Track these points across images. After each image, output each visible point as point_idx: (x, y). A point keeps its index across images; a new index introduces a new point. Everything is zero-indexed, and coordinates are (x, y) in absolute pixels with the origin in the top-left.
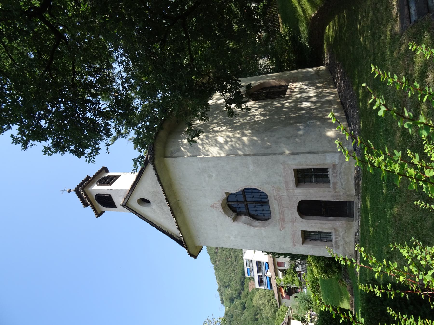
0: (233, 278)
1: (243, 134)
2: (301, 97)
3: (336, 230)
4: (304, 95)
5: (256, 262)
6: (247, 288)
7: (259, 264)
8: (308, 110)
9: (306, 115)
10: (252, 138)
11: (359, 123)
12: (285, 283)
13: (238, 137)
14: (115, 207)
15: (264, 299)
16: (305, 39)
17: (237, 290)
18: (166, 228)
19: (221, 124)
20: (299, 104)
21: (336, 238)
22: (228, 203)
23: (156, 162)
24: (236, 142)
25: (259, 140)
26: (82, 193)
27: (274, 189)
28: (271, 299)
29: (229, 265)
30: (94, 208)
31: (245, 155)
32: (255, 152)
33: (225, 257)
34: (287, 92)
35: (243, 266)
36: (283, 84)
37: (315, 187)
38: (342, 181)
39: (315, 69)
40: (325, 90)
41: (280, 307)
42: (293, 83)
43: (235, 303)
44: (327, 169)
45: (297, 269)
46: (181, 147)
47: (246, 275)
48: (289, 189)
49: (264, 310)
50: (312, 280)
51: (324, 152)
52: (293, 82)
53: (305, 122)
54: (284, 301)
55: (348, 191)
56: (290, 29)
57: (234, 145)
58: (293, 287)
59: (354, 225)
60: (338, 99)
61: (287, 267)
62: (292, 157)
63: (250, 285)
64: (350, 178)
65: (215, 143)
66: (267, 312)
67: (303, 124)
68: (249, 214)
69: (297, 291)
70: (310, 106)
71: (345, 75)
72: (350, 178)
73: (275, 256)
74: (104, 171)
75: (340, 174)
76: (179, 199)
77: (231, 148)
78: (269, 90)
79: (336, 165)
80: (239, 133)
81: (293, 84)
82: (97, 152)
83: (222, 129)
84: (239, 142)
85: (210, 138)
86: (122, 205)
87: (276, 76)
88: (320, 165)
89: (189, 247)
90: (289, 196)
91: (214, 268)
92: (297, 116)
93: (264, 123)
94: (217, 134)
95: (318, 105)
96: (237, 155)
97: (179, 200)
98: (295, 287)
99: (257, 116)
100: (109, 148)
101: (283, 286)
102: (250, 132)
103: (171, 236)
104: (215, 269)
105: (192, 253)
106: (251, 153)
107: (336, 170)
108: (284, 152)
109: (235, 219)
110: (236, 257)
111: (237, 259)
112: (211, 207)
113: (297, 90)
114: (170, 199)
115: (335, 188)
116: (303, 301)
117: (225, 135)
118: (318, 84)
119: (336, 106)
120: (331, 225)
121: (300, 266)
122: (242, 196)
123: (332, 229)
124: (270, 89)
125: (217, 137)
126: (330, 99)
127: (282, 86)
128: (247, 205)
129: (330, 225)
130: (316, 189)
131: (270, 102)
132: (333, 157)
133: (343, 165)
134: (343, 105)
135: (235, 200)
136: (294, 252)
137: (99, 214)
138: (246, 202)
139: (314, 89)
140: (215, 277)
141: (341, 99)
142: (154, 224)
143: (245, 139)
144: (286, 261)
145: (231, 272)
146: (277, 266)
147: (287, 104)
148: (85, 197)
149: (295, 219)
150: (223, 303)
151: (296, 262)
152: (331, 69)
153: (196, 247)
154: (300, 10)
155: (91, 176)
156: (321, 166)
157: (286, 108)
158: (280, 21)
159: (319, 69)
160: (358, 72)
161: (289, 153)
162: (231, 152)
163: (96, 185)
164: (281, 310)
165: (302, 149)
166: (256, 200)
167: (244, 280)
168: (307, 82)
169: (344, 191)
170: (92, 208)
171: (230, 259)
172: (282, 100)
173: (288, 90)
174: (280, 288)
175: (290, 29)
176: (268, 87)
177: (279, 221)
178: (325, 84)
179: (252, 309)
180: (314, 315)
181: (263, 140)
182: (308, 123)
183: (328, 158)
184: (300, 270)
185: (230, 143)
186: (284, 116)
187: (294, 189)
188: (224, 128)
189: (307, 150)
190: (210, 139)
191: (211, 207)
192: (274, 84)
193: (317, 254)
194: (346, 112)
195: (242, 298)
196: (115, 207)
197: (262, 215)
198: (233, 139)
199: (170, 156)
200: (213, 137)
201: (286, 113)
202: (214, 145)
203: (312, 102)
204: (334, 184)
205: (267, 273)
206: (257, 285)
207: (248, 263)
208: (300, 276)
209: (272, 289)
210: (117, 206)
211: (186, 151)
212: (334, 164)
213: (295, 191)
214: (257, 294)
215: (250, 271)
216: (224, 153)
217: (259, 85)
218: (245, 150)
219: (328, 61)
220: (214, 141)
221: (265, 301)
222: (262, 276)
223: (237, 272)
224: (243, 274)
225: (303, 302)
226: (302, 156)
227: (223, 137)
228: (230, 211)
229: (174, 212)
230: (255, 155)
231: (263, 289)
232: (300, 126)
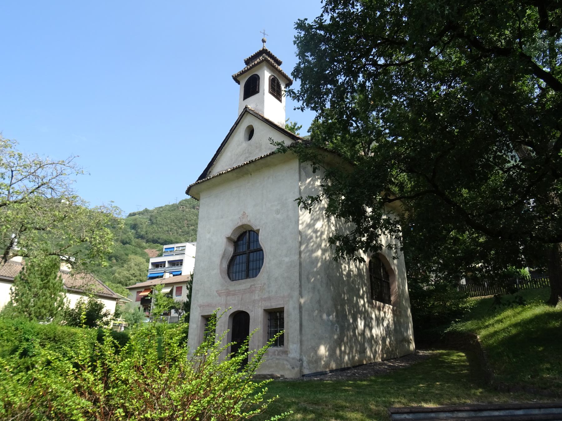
0: (162, 229)
1: (324, 251)
2: (372, 318)
4: (374, 323)
5: (182, 260)
6: (149, 247)
7: (180, 263)
8: (354, 326)
9: (346, 323)
10: (320, 260)
11: (331, 380)
12: (156, 295)
13: (321, 245)
14: (245, 98)
15: (136, 269)
16: (456, 327)
17: (146, 234)
18: (219, 158)
19: (339, 224)
20: (361, 316)
22: (248, 231)
24: (315, 243)
25: (317, 269)
26: (261, 58)
28: (136, 278)
29: (178, 224)
30: (243, 73)
31: (300, 253)
32: (304, 264)
33: (189, 219)
34: (380, 303)
35: (177, 243)
36: (393, 298)
37: (264, 331)
38: (270, 361)
39: (411, 337)
40: (381, 347)
41: (127, 289)
42: (392, 310)
43: (131, 232)
44: (283, 345)
45: (173, 311)
46: (310, 179)
47: (165, 247)
49: (123, 268)
50: (160, 329)
51: (301, 342)
52: (393, 311)
53: (337, 322)
54: (134, 294)
56: (470, 309)
57: (312, 240)
58: (152, 305)
60: (367, 362)
61: (176, 298)
62: (297, 306)
63: (153, 250)
65: (315, 219)
66: (121, 272)
67: (335, 319)
68: (236, 256)
69: (146, 311)
70: (359, 328)
71: (393, 369)
72: (272, 370)
73: (189, 284)
75: (277, 359)
77: (309, 237)
78: (384, 281)
79: (287, 354)
80: (326, 246)
81: (390, 311)
82: (294, 98)
83: (332, 226)
84: (315, 246)
85: (321, 212)
86: (246, 107)
87: (403, 291)
89: (199, 186)
90: (254, 301)
91: (174, 204)
92: (346, 312)
93: (338, 275)
94: (326, 220)
95: (360, 338)
96: (301, 244)
97: (251, 174)
98: (151, 308)
99: (347, 266)
100: (300, 110)
101: (153, 293)
102: (328, 258)
103: (211, 165)
104: (173, 205)
105: (192, 189)
106: (302, 260)
107: (281, 355)
108: (302, 297)
109: (229, 239)
110: (188, 233)
111: (185, 234)
113: (382, 314)
114: (252, 165)
116: (135, 317)
117: (325, 229)
118: (388, 340)
119: (357, 358)
121: (177, 315)
122: (255, 248)
124: (386, 282)
125: (322, 220)
126: (367, 352)
127: (390, 297)
128: (245, 254)
131: (366, 282)
132: (296, 352)
134: (359, 366)
135: (252, 240)
136: (193, 306)
137: (236, 79)
138: (249, 253)
139: (381, 335)
140: (163, 205)
141: (366, 364)
142: (225, 144)
143: (319, 253)
144: (183, 298)
145: (169, 226)
146: (177, 287)
147: (362, 302)
148: (256, 62)
150: (130, 215)
151: (182, 310)
152: (408, 356)
153: (198, 194)
154: (491, 321)
155: (280, 68)
157: (357, 300)
158: (487, 297)
159: (411, 343)
160: (389, 382)
161: (301, 303)
162: (303, 237)
163: (270, 75)
164: (123, 290)
165: (305, 317)
166: (251, 264)
167: (159, 243)
168: (392, 327)
170: (244, 70)
171: (185, 225)
172: (369, 296)
173: (382, 304)
174: (150, 289)
175: (470, 309)
176: (388, 280)
177: (227, 289)
178: (388, 348)
179: (122, 252)
180: (121, 329)
181: (318, 273)
182: (337, 325)
183: (295, 346)
184: (172, 315)
185: (314, 235)
186: (346, 298)
188: (333, 228)
189: (305, 323)
190: (320, 213)
192: (392, 288)
193: (190, 331)
194: (348, 368)
195: (137, 240)
196: (245, 98)
197: (234, 271)
198: (319, 239)
199: (301, 165)
200: (322, 216)
201: (350, 300)
202: (313, 217)
203: (364, 331)
205: (169, 274)
206: (153, 260)
207: (181, 248)
208: (165, 314)
209: (149, 279)
210: (246, 100)
211: (306, 185)
213: (260, 309)
214: (142, 260)
215: (171, 251)
216: (303, 229)
217: (392, 269)
218: (306, 253)
219: (421, 354)
220: (318, 217)
221: (134, 270)
222: (164, 266)
223: (169, 234)
224: (166, 243)
225: (133, 317)
227: (322, 227)
228: (239, 234)
229: (238, 170)
230: (300, 264)
231: (148, 268)
232: (333, 316)
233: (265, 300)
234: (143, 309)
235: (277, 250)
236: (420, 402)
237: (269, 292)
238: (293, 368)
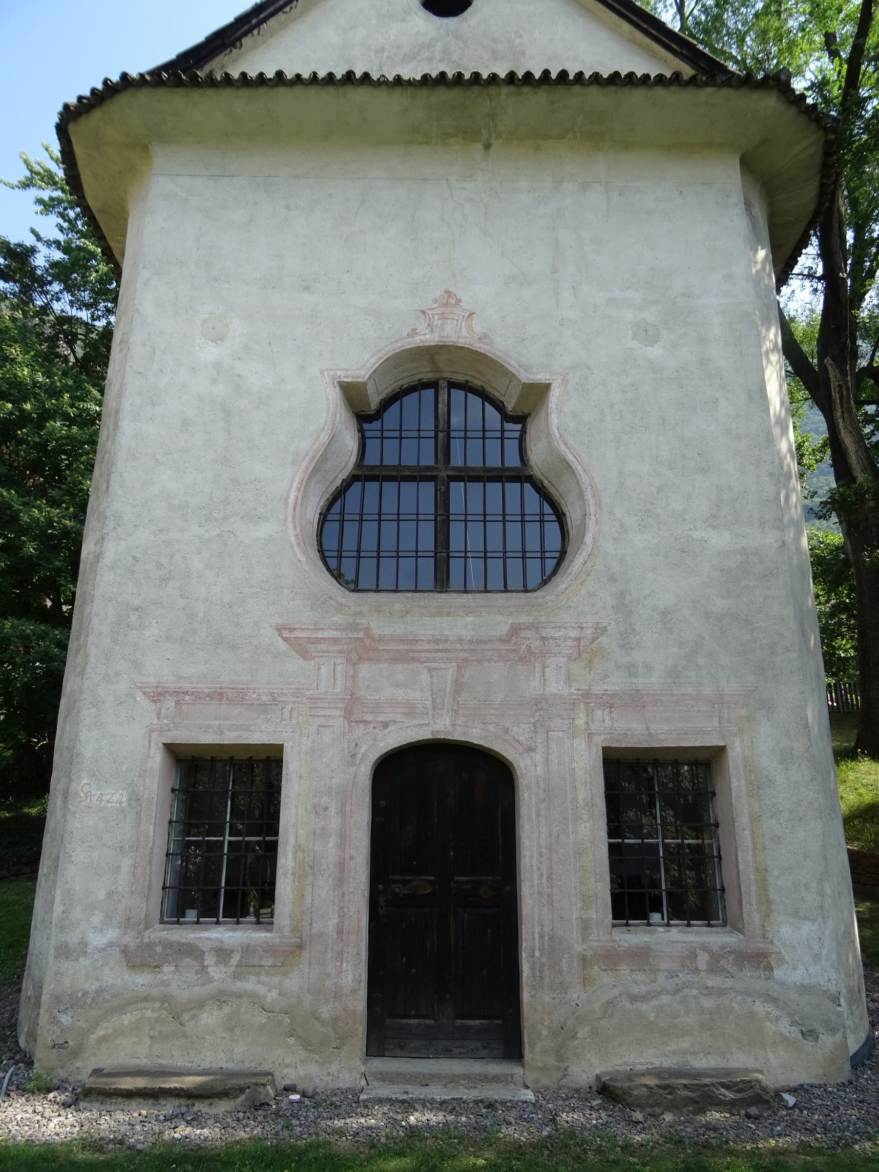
21: (223, 954)
27: (589, 632)
38: (665, 999)
48: (590, 713)
55: (595, 1033)
59: (334, 1068)
64: (685, 1043)
72: (685, 1043)
75: (709, 991)
76: (492, 150)
79: (769, 968)
90: (540, 703)
97: (487, 146)
107: (733, 970)
112: (448, 292)
120: (331, 931)
123: (295, 929)
132: (817, 958)
133: (770, 1008)
149: (368, 717)
169: (596, 1006)
183: (808, 928)
187: (590, 736)
212: (773, 960)
213: (580, 743)
233: (609, 703)
235: (660, 489)
237: (630, 669)
238: (810, 1034)
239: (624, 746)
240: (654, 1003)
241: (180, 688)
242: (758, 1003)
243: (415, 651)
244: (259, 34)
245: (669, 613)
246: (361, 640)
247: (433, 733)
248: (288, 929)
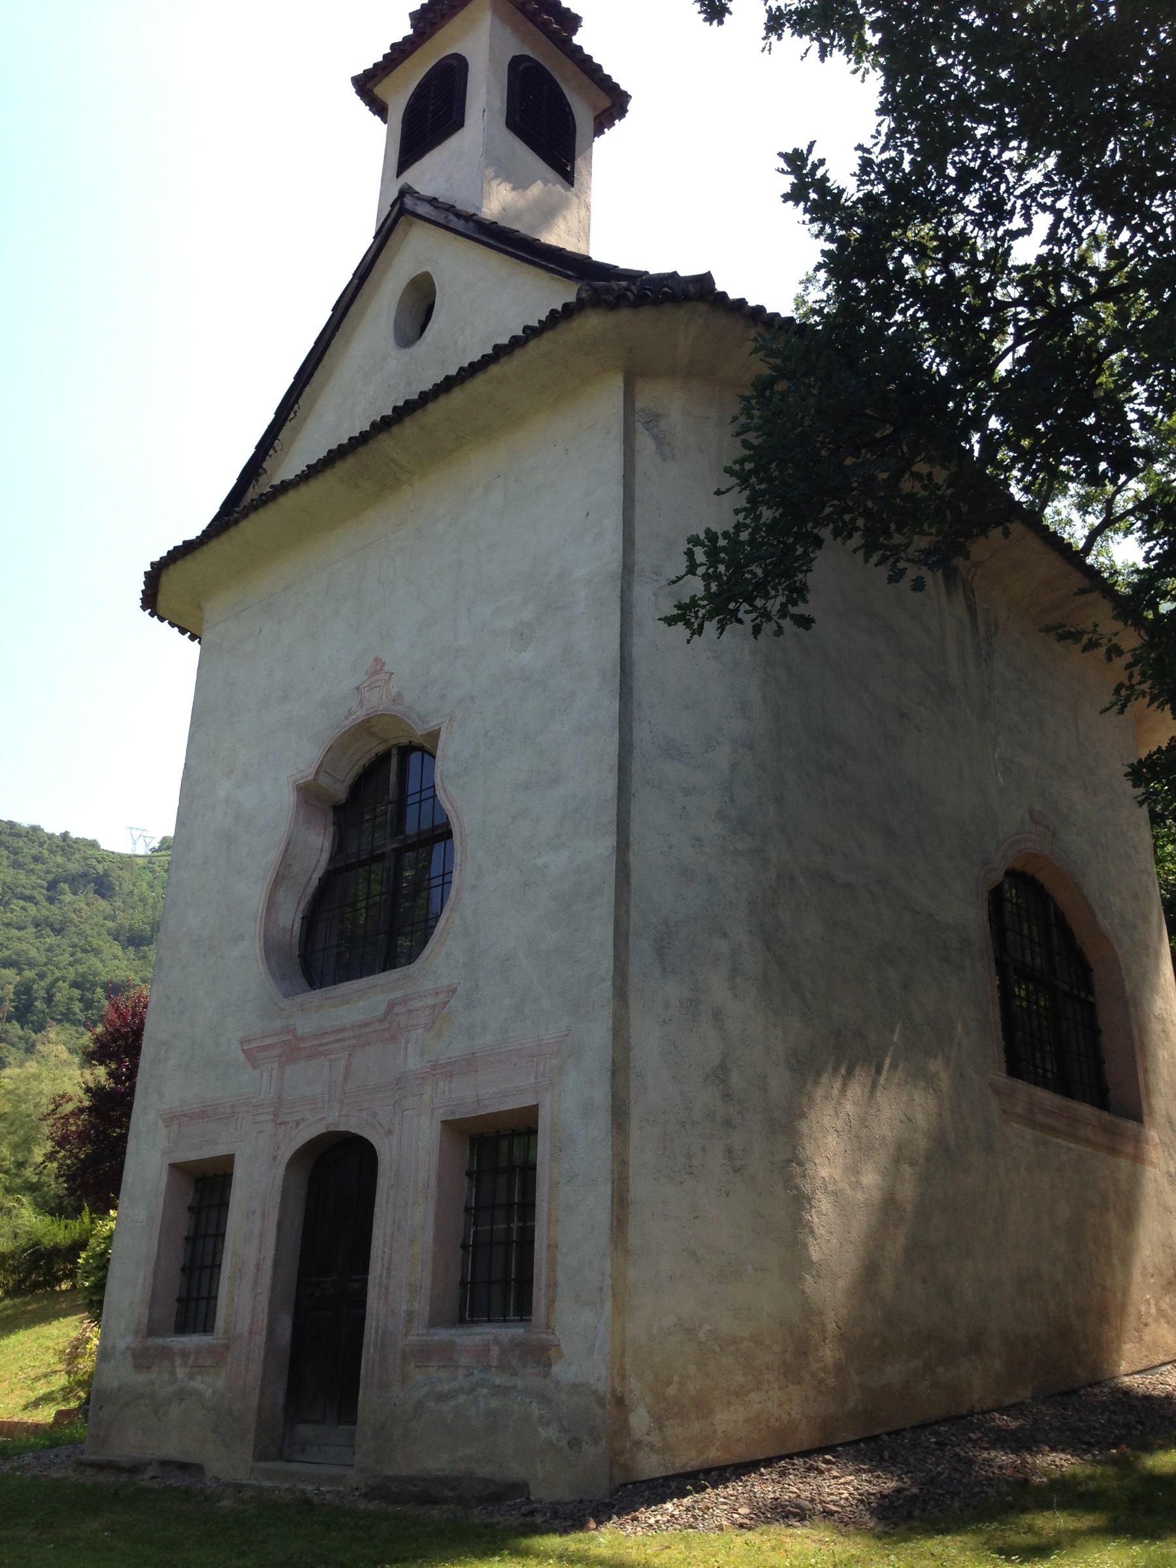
3: (220, 1354)
21: (184, 1354)
22: (394, 751)
23: (592, 322)
38: (462, 1399)
74: (605, 103)
79: (549, 1365)
88: (553, 1264)
112: (376, 660)
115: (424, 1353)
123: (226, 1331)
129: (248, 1322)
130: (427, 1239)
149: (288, 1118)
156: (544, 1270)
189: (639, 1189)
191: (376, 660)
204: (446, 1352)
210: (401, 178)
226: (604, 1153)
234: (886, 1492)
236: (609, 281)
239: (457, 1118)
240: (453, 1403)
241: (182, 1111)
242: (534, 1405)
243: (322, 1045)
244: (276, 452)
245: (508, 960)
246: (290, 1041)
247: (328, 1126)
248: (222, 1331)
